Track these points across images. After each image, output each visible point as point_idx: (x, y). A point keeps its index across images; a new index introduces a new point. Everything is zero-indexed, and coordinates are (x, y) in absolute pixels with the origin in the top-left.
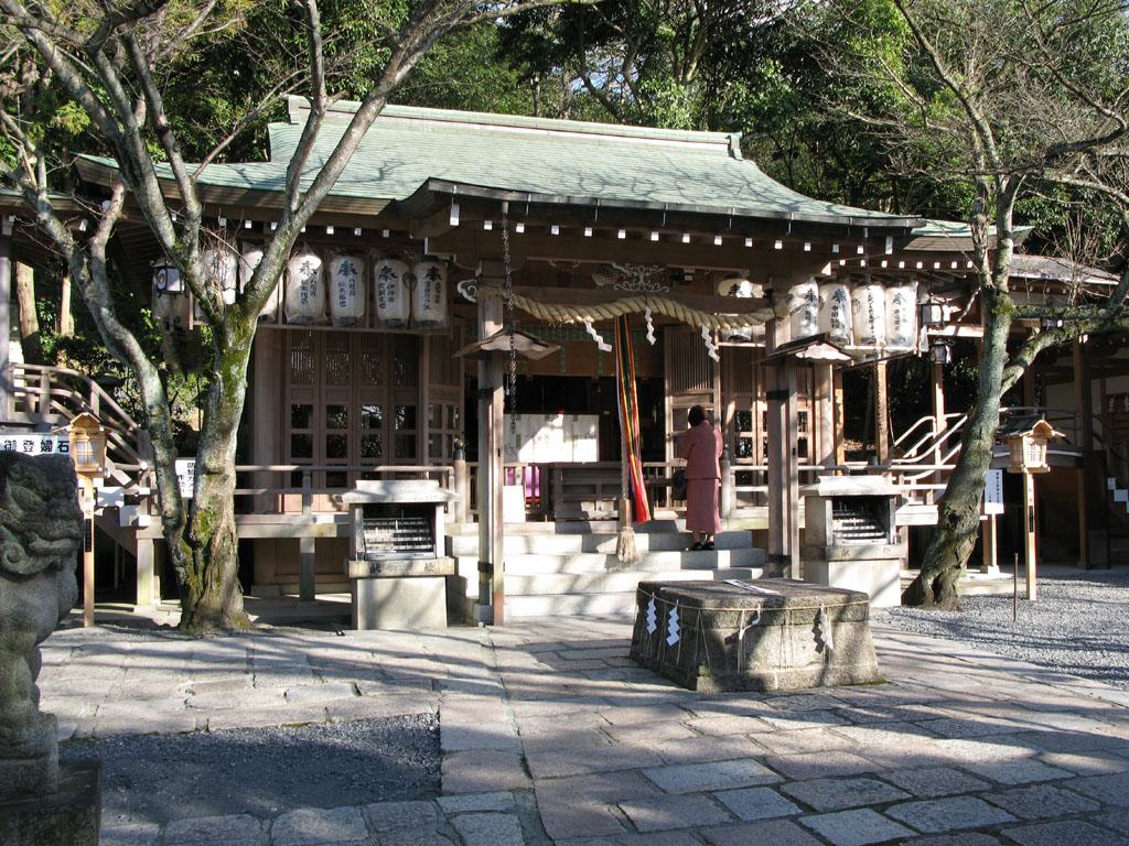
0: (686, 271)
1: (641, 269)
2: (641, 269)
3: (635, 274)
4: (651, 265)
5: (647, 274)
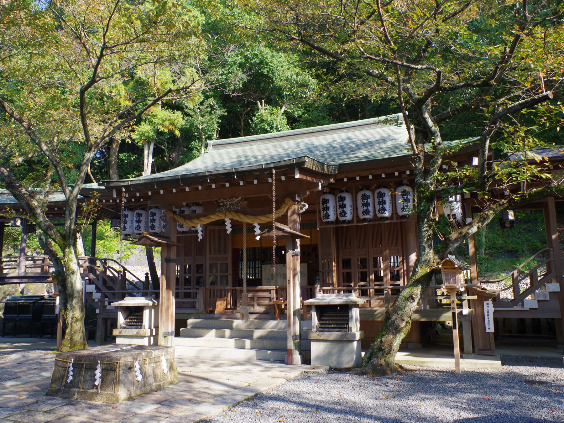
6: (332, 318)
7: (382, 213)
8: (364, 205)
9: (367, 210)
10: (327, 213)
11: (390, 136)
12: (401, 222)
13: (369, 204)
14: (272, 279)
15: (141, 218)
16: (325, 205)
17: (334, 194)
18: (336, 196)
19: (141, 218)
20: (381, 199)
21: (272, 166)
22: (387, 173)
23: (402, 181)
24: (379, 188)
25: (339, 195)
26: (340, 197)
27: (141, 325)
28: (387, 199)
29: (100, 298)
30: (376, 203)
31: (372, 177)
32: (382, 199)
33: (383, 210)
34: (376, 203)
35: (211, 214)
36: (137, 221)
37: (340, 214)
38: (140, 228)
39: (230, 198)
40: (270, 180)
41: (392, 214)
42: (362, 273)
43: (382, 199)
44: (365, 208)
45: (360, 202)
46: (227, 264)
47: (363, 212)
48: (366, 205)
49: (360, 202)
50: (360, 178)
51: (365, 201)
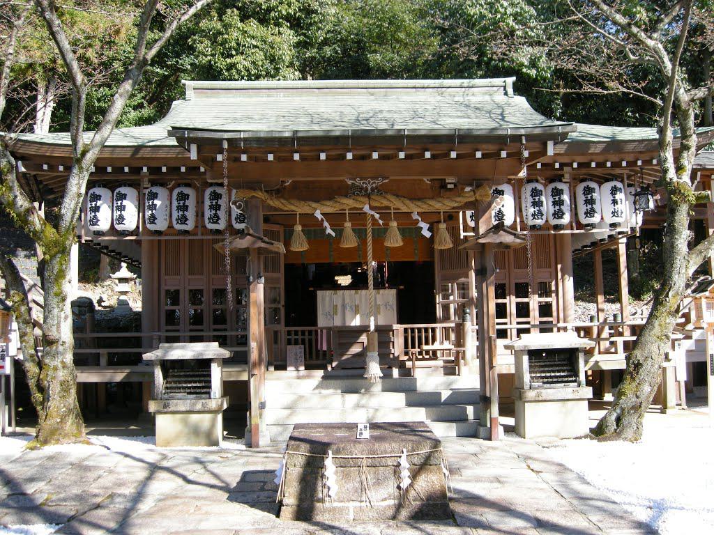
0: (447, 181)
1: (369, 182)
2: (369, 182)
3: (365, 185)
4: (377, 178)
5: (374, 185)
9: (560, 210)
10: (95, 216)
12: (159, 241)
13: (187, 206)
15: (187, 203)
16: (181, 203)
17: (110, 188)
18: (171, 191)
19: (187, 203)
21: (523, 132)
22: (463, 162)
25: (117, 191)
26: (119, 193)
28: (191, 203)
29: (591, 396)
30: (174, 208)
31: (186, 169)
32: (559, 198)
33: (559, 214)
34: (174, 208)
35: (432, 198)
37: (90, 221)
38: (187, 219)
39: (373, 178)
40: (219, 158)
41: (196, 227)
42: (288, 339)
43: (559, 198)
45: (581, 198)
47: (553, 215)
48: (216, 207)
49: (581, 198)
51: (537, 199)
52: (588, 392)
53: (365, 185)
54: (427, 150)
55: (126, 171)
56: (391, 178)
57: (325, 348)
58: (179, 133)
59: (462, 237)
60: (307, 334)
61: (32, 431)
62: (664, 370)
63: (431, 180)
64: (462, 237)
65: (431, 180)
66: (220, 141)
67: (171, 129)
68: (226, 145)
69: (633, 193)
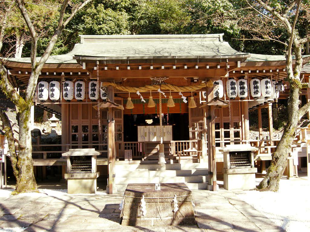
0: (194, 79)
1: (160, 79)
2: (160, 79)
3: (158, 80)
4: (164, 77)
5: (162, 80)
6: (243, 160)
7: (243, 95)
8: (255, 88)
11: (208, 46)
12: (69, 104)
13: (81, 89)
14: (146, 136)
15: (81, 88)
16: (79, 88)
17: (48, 82)
18: (74, 83)
19: (81, 88)
20: (242, 86)
21: (227, 57)
22: (201, 70)
23: (244, 76)
24: (78, 80)
25: (51, 83)
27: (91, 170)
28: (83, 88)
30: (76, 90)
32: (243, 86)
34: (76, 90)
36: (78, 90)
38: (81, 95)
39: (162, 77)
43: (243, 86)
44: (242, 90)
45: (252, 86)
46: (121, 125)
48: (94, 90)
49: (252, 86)
50: (81, 73)
52: (255, 170)
53: (158, 80)
54: (186, 65)
55: (174, 68)
56: (170, 77)
57: (141, 151)
58: (78, 58)
59: (200, 103)
60: (133, 145)
61: (14, 187)
62: (288, 160)
63: (187, 78)
64: (200, 103)
65: (187, 78)
66: (96, 61)
67: (74, 56)
68: (98, 63)
69: (275, 84)
